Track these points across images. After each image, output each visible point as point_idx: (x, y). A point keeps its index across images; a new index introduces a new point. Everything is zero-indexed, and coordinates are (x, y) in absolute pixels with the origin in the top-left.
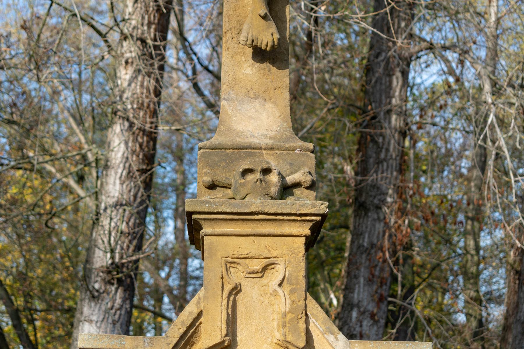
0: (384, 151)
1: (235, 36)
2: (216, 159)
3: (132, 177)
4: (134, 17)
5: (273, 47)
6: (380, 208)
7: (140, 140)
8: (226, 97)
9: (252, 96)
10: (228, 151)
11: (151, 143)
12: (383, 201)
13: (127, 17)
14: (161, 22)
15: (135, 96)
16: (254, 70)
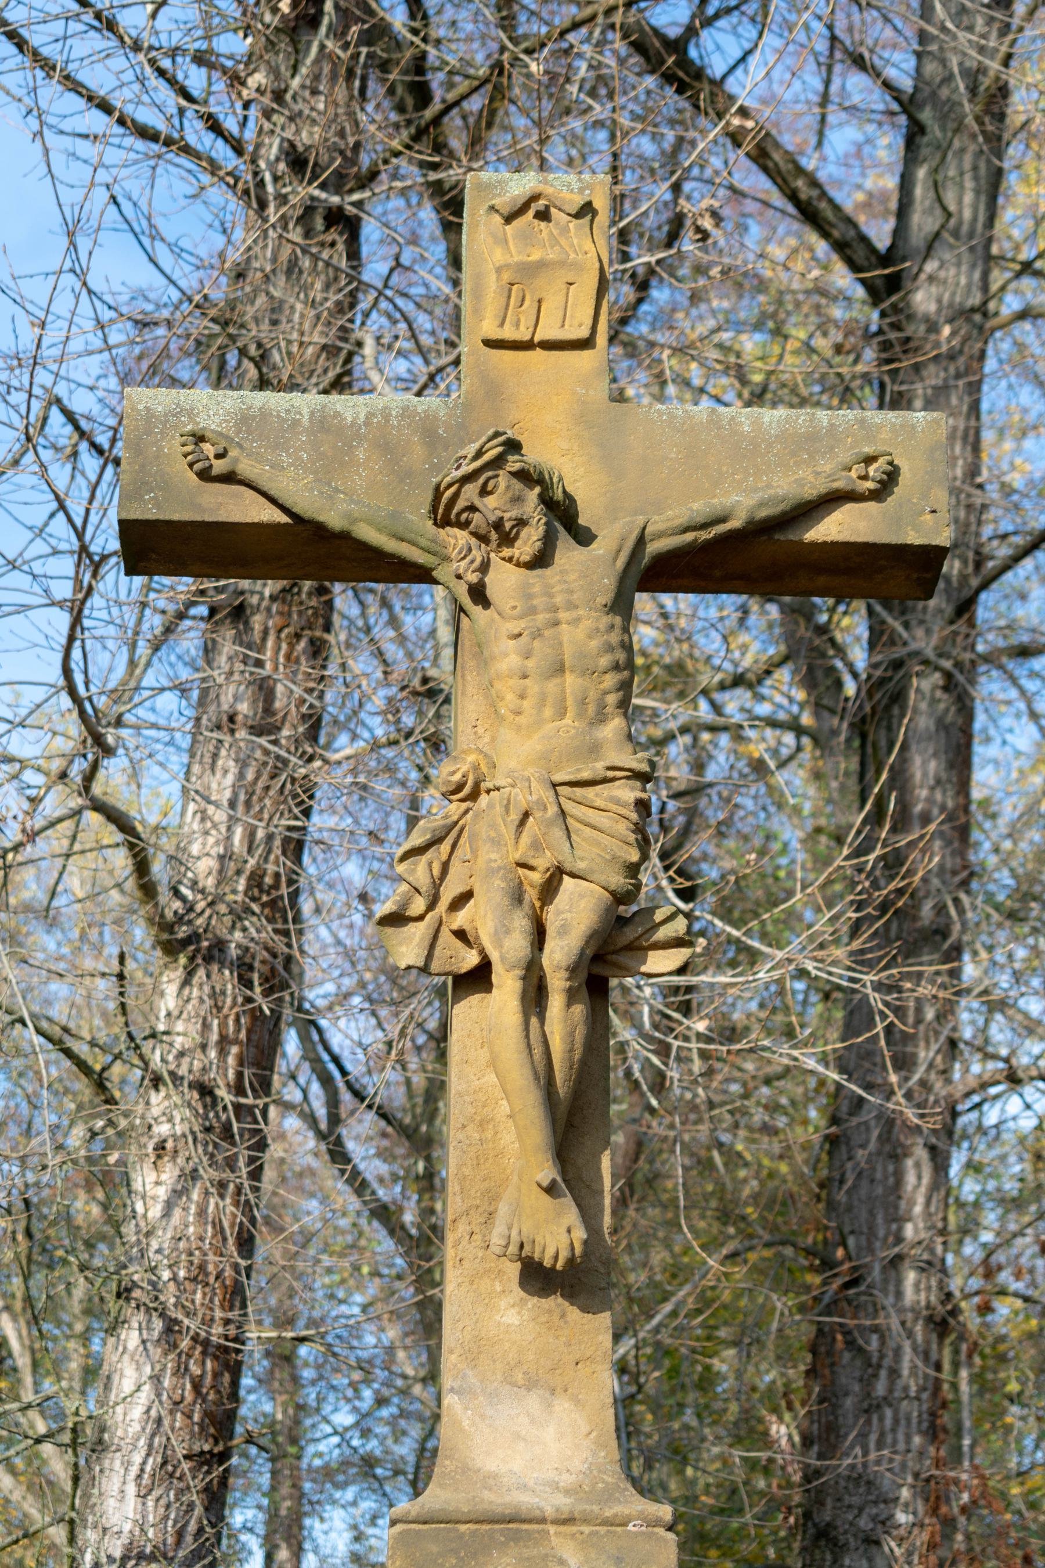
0: (883, 1373)
1: (476, 1229)
2: (434, 1548)
3: (171, 1475)
4: (180, 1027)
5: (571, 1261)
6: (877, 1543)
7: (195, 1370)
8: (456, 1385)
9: (521, 1382)
10: (463, 1528)
11: (227, 1378)
12: (883, 1523)
13: (161, 1027)
14: (255, 1037)
15: (182, 1245)
16: (526, 1315)
